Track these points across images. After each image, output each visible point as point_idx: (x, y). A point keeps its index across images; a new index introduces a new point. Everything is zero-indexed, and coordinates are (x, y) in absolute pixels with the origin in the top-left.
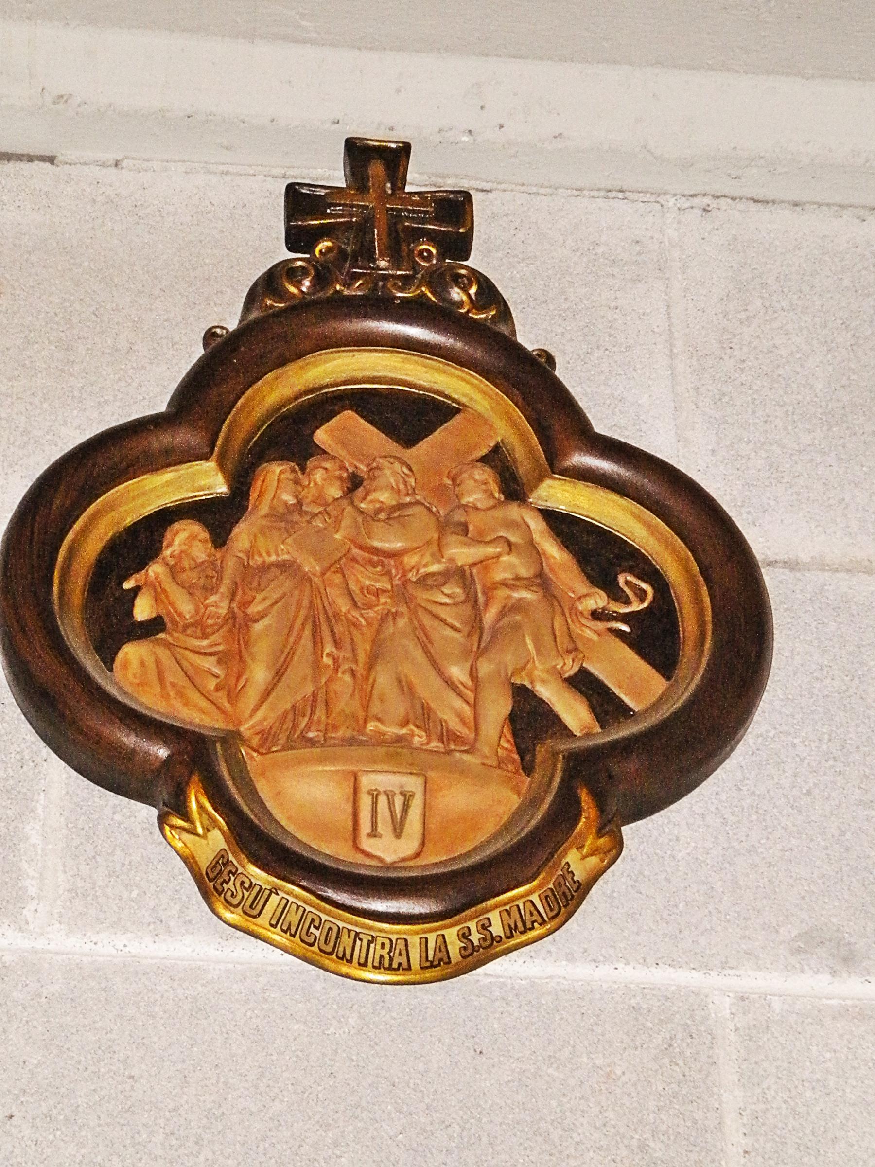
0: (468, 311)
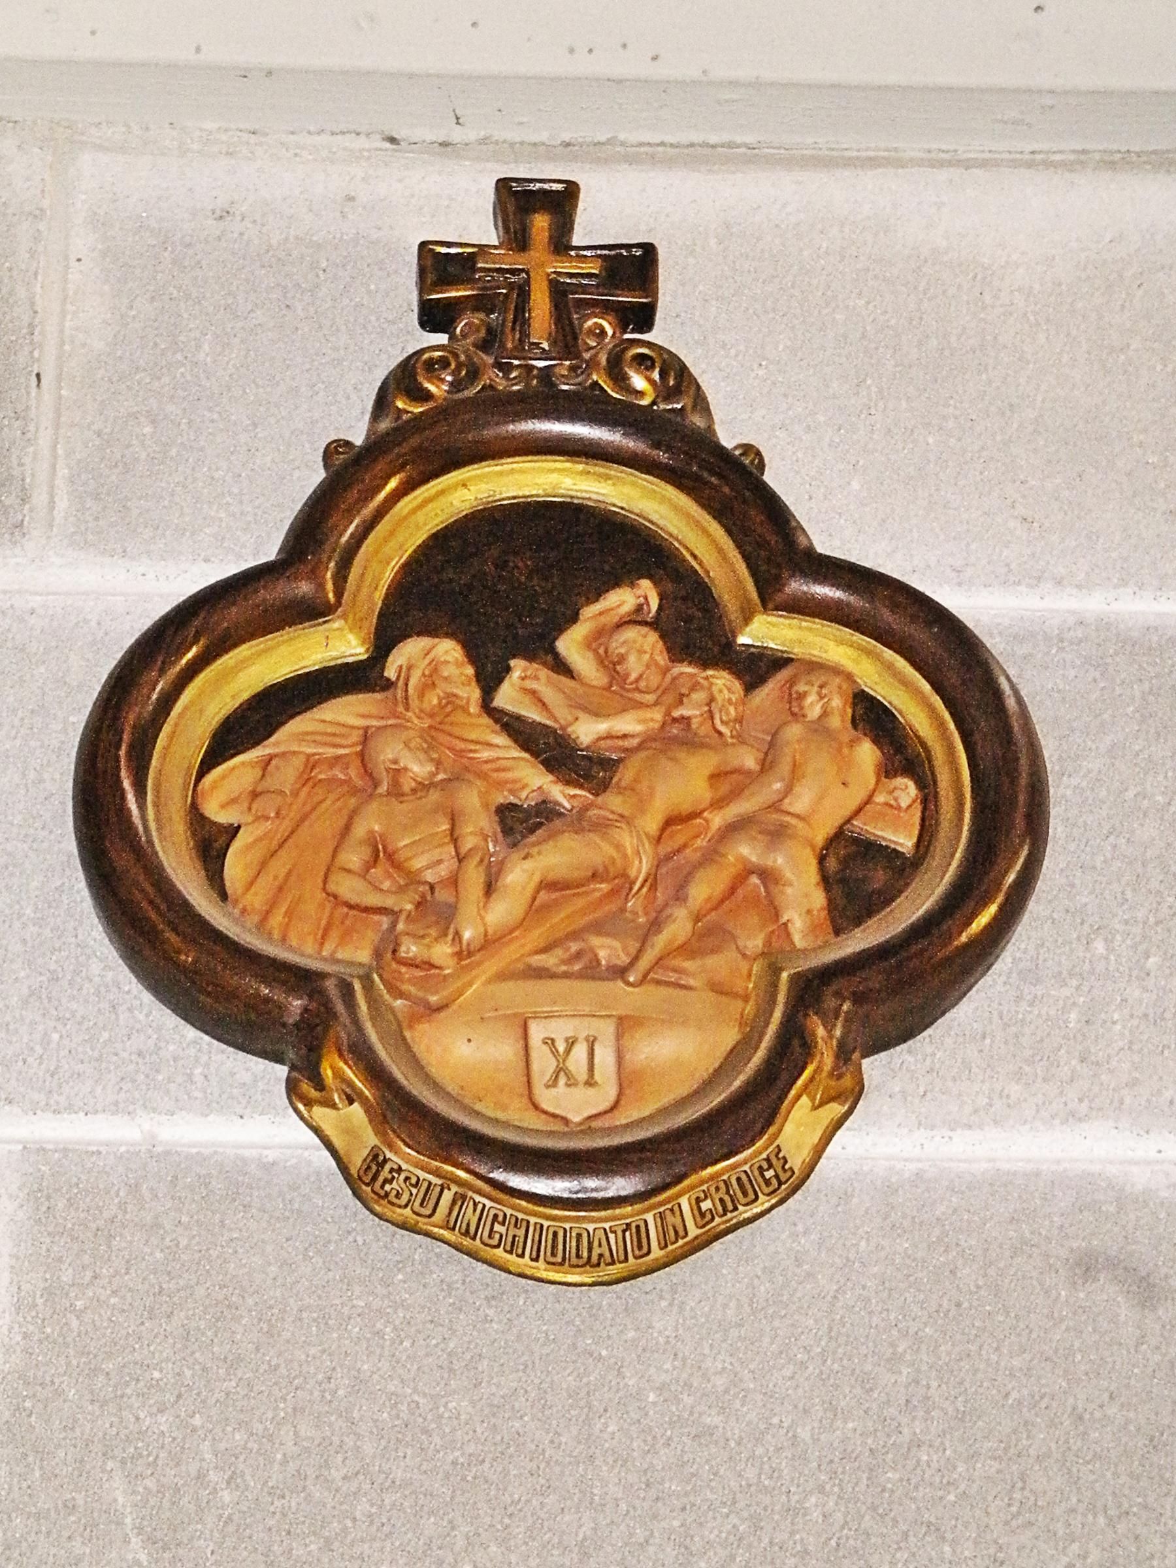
0: (654, 403)
